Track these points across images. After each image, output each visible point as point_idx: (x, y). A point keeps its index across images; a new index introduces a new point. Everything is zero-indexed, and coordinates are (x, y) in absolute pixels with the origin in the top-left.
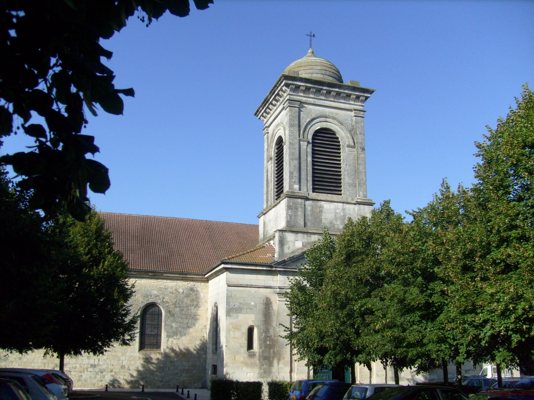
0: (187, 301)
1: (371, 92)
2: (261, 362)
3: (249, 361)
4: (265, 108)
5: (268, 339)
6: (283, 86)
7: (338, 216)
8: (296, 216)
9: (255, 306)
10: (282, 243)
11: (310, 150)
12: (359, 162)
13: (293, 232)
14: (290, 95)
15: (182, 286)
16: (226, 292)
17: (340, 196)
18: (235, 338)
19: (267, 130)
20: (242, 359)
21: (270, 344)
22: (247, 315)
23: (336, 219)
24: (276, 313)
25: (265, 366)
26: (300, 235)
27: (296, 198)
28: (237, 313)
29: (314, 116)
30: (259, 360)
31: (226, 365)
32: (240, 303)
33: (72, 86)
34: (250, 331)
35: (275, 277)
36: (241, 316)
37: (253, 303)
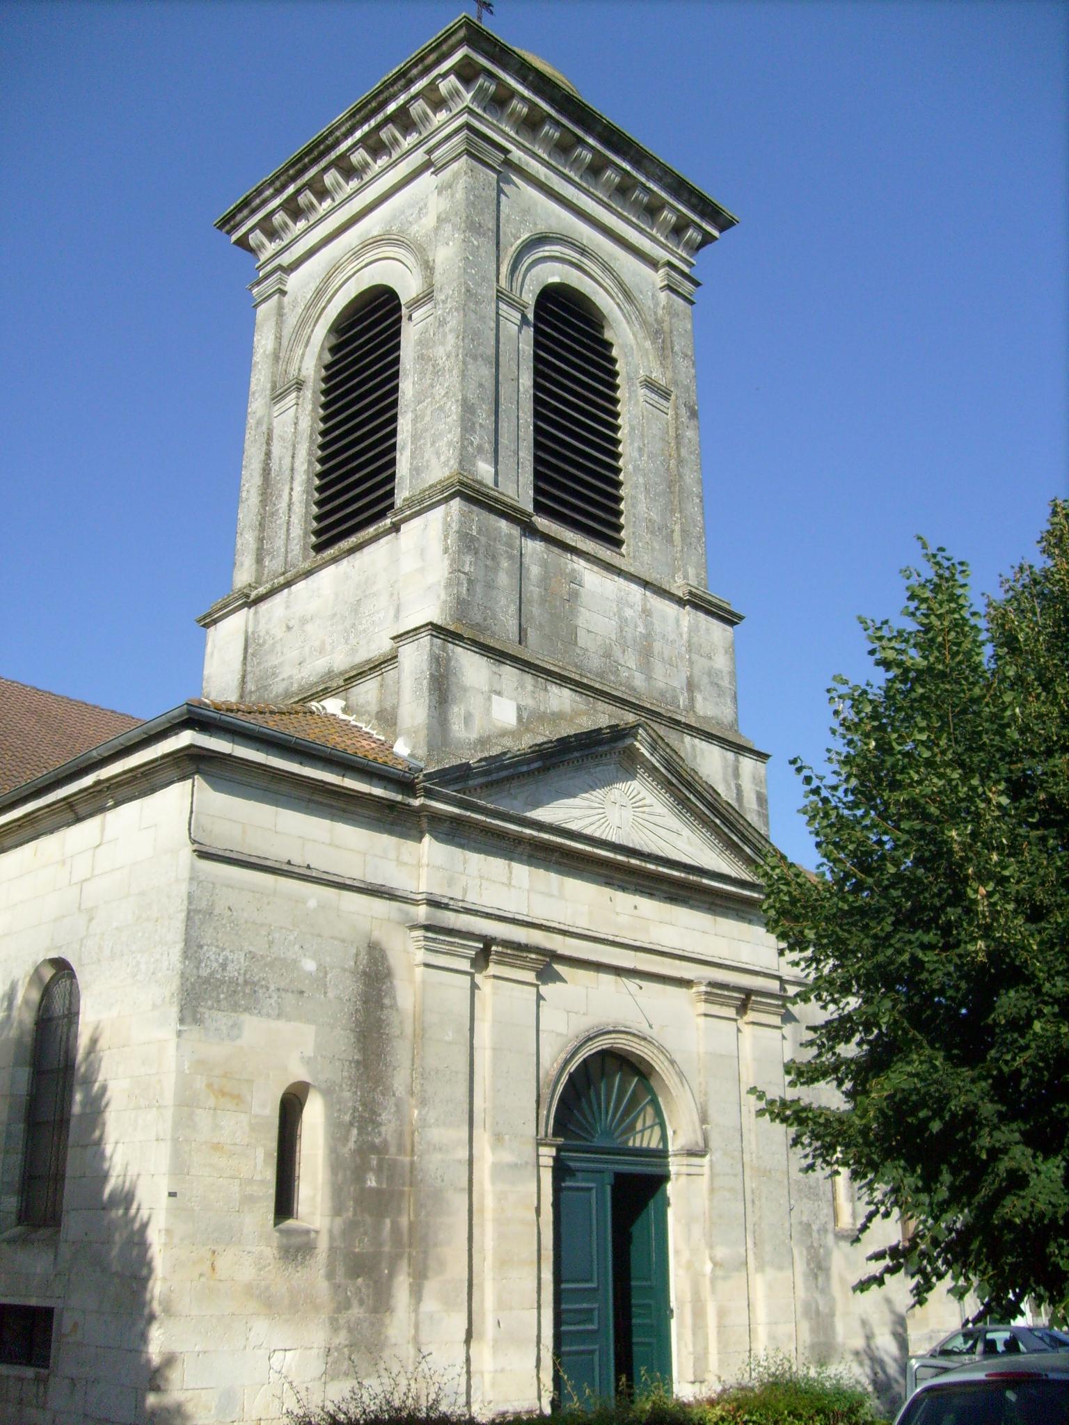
1: (725, 224)
2: (336, 1288)
3: (281, 1280)
4: (291, 189)
5: (374, 1160)
6: (444, 76)
8: (490, 586)
9: (320, 980)
10: (442, 687)
11: (527, 348)
13: (486, 650)
14: (471, 112)
16: (184, 888)
18: (217, 1147)
19: (281, 281)
20: (247, 1273)
21: (378, 1192)
22: (281, 1024)
24: (409, 1030)
25: (356, 1312)
27: (492, 510)
28: (235, 1007)
29: (542, 228)
30: (330, 1275)
31: (167, 1310)
32: (252, 956)
34: (290, 1108)
35: (411, 844)
36: (254, 1028)
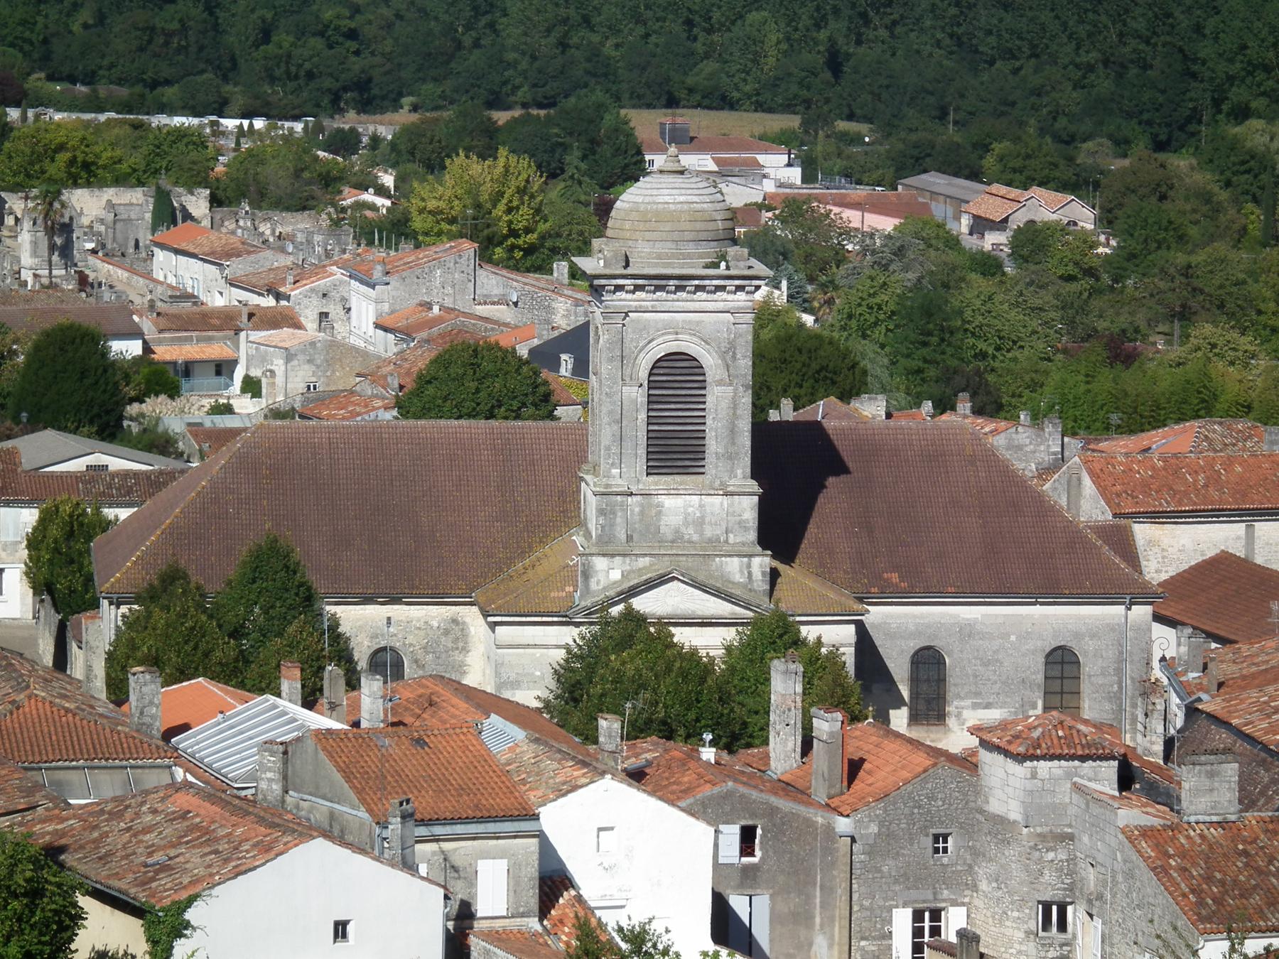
0: (447, 642)
7: (690, 519)
8: (612, 525)
12: (739, 412)
13: (604, 555)
15: (435, 614)
17: (700, 477)
23: (686, 523)
26: (618, 560)
33: (897, 221)
37: (538, 673)
